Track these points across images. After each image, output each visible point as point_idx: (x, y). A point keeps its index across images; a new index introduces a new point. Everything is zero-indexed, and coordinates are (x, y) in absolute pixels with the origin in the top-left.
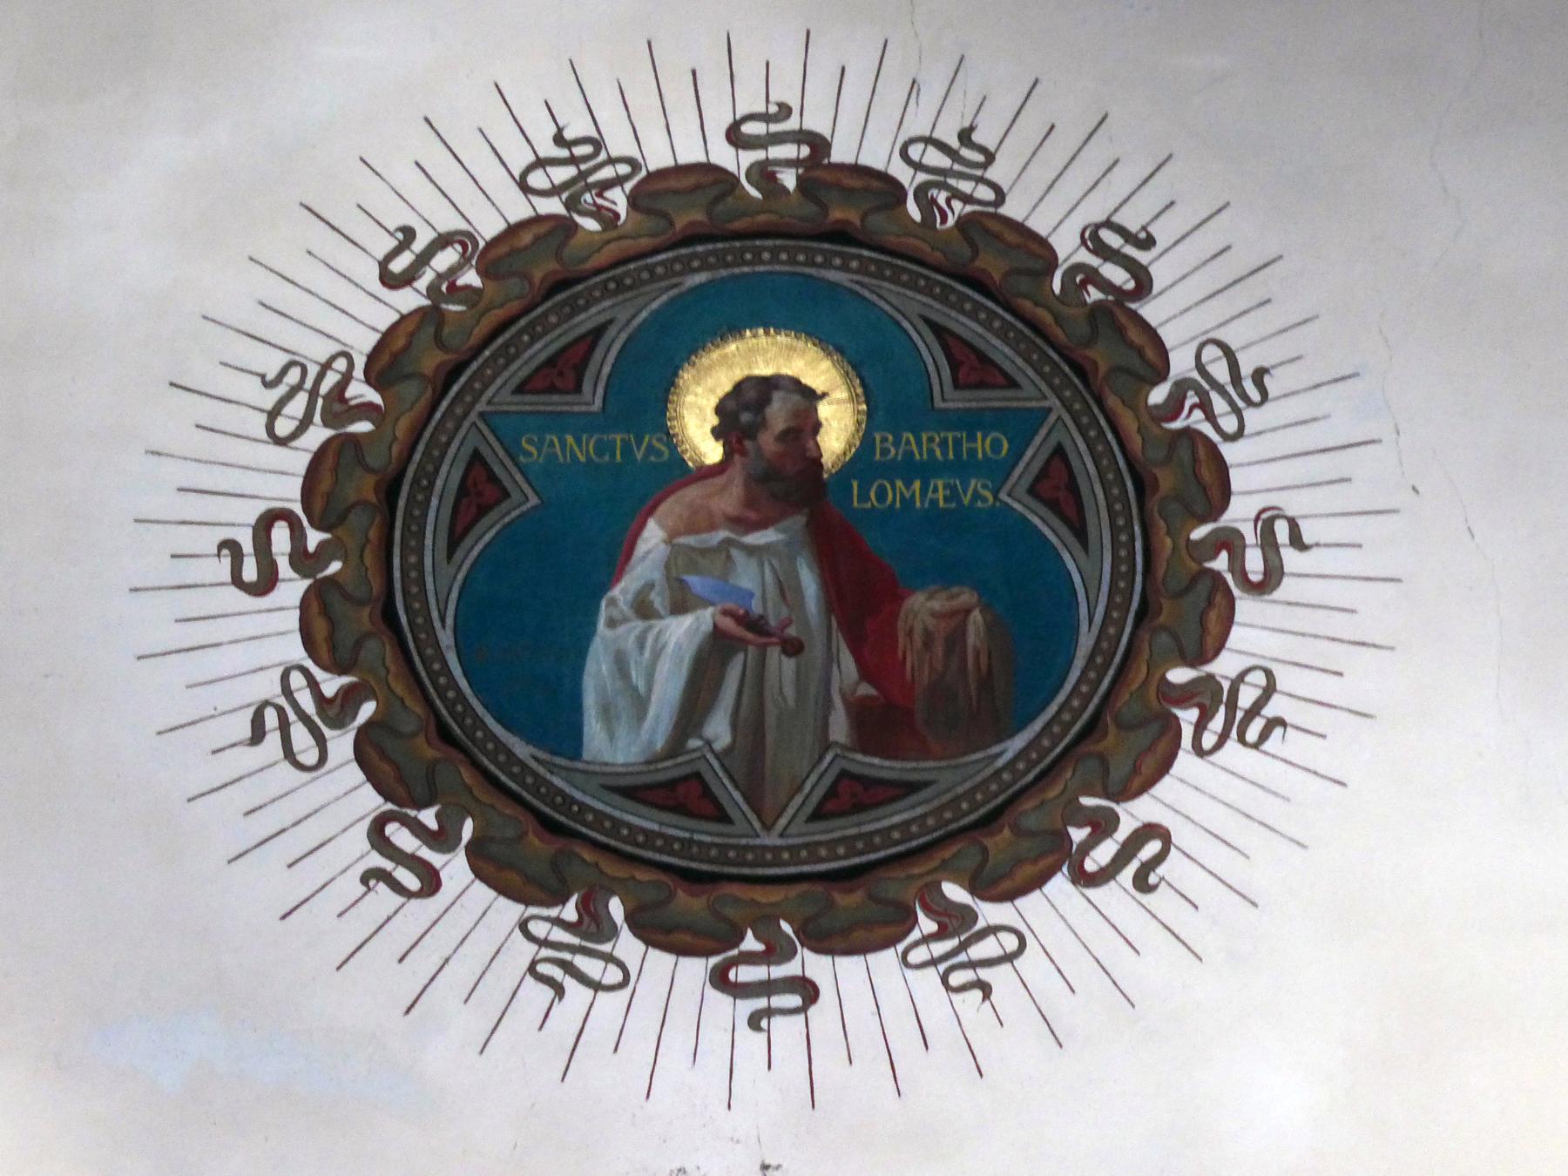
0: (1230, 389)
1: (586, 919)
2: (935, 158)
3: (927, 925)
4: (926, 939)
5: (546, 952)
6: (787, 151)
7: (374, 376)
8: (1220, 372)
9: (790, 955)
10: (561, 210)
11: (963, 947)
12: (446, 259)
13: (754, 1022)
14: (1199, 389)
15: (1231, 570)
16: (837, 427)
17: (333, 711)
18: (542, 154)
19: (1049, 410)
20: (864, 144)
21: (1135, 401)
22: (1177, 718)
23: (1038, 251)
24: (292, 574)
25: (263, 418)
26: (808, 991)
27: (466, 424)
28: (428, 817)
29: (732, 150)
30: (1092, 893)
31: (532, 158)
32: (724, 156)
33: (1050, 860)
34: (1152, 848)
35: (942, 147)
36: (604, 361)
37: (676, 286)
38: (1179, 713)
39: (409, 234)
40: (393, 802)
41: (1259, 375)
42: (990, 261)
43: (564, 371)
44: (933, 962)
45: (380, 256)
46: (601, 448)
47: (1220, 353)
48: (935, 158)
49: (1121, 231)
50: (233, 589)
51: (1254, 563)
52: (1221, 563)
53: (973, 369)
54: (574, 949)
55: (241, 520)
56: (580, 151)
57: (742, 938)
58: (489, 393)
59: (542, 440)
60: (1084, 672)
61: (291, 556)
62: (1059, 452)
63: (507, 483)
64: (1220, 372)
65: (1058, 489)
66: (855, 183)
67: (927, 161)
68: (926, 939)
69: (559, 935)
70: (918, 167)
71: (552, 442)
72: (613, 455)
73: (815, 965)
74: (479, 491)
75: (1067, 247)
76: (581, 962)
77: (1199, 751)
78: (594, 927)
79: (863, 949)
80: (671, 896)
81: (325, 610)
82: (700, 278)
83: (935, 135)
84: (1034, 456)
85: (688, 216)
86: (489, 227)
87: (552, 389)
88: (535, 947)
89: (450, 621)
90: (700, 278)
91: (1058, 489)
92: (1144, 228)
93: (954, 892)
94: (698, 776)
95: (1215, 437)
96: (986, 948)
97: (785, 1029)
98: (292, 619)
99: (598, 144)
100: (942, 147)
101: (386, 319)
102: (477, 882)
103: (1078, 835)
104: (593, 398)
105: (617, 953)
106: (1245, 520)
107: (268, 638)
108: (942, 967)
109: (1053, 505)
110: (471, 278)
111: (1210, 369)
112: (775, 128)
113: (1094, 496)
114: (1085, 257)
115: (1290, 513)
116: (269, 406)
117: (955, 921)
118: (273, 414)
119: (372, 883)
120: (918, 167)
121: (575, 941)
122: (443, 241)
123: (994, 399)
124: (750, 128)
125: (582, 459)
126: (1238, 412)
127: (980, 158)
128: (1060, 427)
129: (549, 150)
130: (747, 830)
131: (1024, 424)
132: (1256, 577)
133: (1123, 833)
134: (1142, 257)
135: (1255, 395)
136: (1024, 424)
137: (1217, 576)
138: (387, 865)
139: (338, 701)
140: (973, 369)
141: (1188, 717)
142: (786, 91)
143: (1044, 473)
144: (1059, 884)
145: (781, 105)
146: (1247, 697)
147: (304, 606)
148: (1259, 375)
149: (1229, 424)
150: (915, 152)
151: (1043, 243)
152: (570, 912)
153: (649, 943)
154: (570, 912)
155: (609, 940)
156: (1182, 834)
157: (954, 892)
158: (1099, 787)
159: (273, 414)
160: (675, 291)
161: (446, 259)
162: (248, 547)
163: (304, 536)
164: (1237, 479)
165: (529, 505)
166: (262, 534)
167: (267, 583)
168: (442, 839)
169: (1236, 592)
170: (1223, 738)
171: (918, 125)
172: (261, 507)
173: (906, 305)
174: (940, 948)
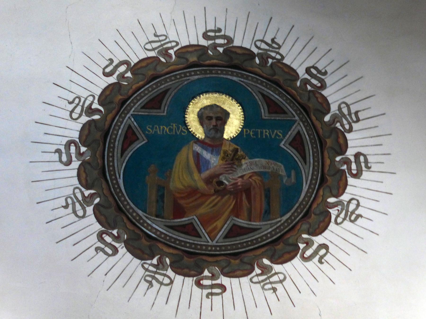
2: (264, 46)
3: (258, 271)
4: (257, 275)
6: (206, 282)
7: (100, 103)
11: (269, 278)
12: (123, 68)
15: (348, 169)
18: (280, 285)
20: (242, 40)
21: (321, 120)
22: (330, 213)
24: (76, 159)
25: (69, 113)
26: (205, 36)
28: (309, 88)
29: (223, 283)
31: (284, 283)
33: (136, 68)
35: (157, 281)
36: (167, 100)
38: (330, 210)
40: (105, 228)
41: (356, 113)
42: (280, 76)
43: (155, 102)
45: (103, 67)
46: (171, 130)
48: (264, 46)
49: (106, 253)
50: (59, 163)
53: (274, 107)
56: (161, 38)
57: (224, 51)
59: (153, 126)
60: (305, 197)
67: (262, 47)
68: (257, 275)
71: (156, 127)
73: (204, 42)
74: (130, 137)
75: (301, 72)
76: (267, 47)
77: (336, 223)
80: (183, 258)
81: (340, 145)
82: (196, 77)
84: (292, 133)
85: (193, 59)
86: (134, 60)
87: (153, 108)
90: (196, 77)
92: (97, 253)
94: (192, 223)
96: (275, 278)
97: (217, 299)
100: (157, 281)
104: (164, 112)
106: (75, 161)
107: (68, 178)
108: (262, 284)
110: (129, 74)
114: (307, 76)
116: (70, 110)
117: (265, 270)
118: (72, 112)
119: (98, 251)
122: (122, 63)
123: (279, 117)
128: (300, 127)
129: (279, 286)
130: (205, 239)
134: (100, 245)
138: (102, 246)
140: (274, 107)
142: (207, 302)
147: (79, 169)
148: (356, 113)
150: (258, 44)
151: (295, 71)
157: (266, 262)
159: (72, 112)
161: (123, 68)
166: (67, 147)
168: (306, 82)
170: (344, 219)
171: (259, 36)
174: (261, 278)
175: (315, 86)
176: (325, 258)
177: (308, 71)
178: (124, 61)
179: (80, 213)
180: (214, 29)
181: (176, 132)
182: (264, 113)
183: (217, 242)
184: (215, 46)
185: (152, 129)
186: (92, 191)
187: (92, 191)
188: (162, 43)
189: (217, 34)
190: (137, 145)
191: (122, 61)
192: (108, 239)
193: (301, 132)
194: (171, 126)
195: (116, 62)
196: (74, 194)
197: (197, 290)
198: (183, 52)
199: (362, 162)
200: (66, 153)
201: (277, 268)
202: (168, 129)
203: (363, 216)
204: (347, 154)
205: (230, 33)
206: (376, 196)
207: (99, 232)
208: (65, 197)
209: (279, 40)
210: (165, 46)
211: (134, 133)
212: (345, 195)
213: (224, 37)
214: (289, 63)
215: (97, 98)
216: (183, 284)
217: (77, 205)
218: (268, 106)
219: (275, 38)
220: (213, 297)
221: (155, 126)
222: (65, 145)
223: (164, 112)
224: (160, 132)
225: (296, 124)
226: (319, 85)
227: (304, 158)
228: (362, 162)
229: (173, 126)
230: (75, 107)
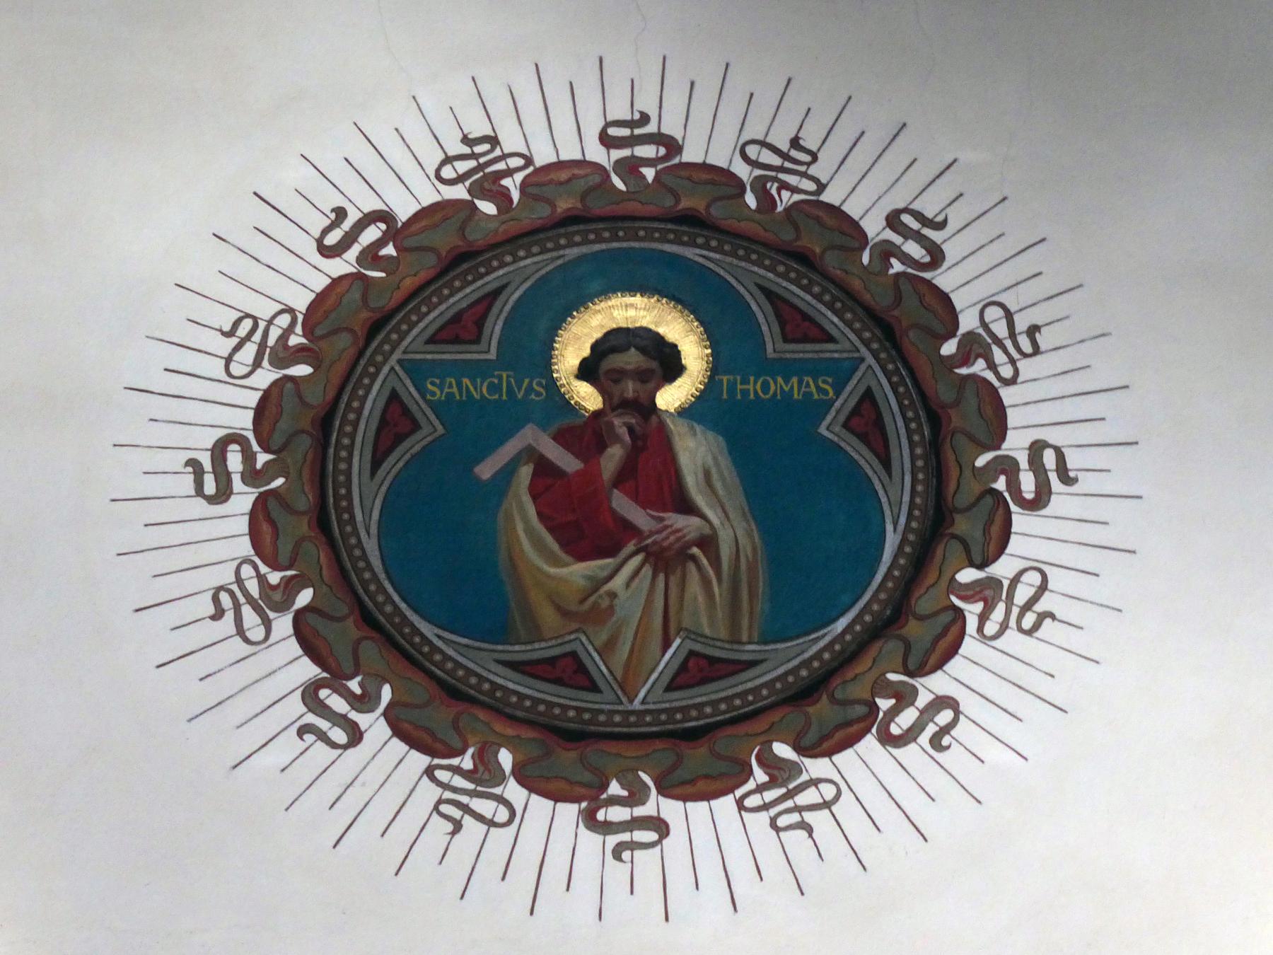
0: (242, 600)
1: (481, 769)
5: (448, 795)
6: (617, 814)
8: (1001, 329)
9: (619, 163)
10: (466, 196)
13: (645, 119)
14: (974, 347)
16: (670, 397)
17: (976, 349)
19: (862, 360)
20: (707, 145)
23: (851, 230)
27: (386, 369)
30: (379, 206)
31: (834, 808)
32: (671, 809)
34: (332, 239)
35: (480, 818)
37: (559, 258)
39: (341, 213)
42: (812, 242)
44: (765, 807)
46: (494, 388)
47: (248, 634)
51: (235, 461)
52: (262, 458)
53: (799, 326)
54: (781, 169)
55: (1062, 500)
58: (405, 343)
61: (1019, 470)
62: (868, 395)
63: (419, 416)
64: (1001, 329)
65: (867, 421)
66: (705, 176)
69: (459, 782)
70: (754, 164)
72: (501, 395)
74: (396, 422)
78: (485, 775)
79: (708, 796)
83: (769, 140)
86: (404, 210)
88: (439, 790)
89: (374, 529)
91: (867, 421)
93: (782, 750)
95: (996, 383)
98: (243, 525)
99: (494, 141)
101: (320, 283)
102: (856, 218)
103: (389, 250)
105: (506, 796)
109: (863, 438)
111: (993, 327)
112: (625, 837)
113: (896, 426)
115: (201, 500)
117: (779, 772)
120: (754, 164)
121: (471, 786)
124: (649, 836)
125: (477, 396)
126: (1013, 362)
127: (807, 158)
128: (873, 373)
131: (841, 374)
132: (1029, 496)
133: (355, 250)
135: (224, 597)
136: (841, 374)
137: (998, 494)
139: (973, 356)
140: (799, 326)
141: (972, 610)
142: (617, 872)
143: (856, 412)
144: (869, 743)
145: (642, 113)
146: (1022, 594)
148: (218, 614)
149: (1007, 372)
150: (752, 151)
151: (855, 225)
152: (467, 763)
153: (531, 790)
154: (467, 763)
155: (499, 785)
156: (968, 703)
157: (782, 750)
158: (901, 670)
160: (560, 262)
162: (207, 465)
163: (1009, 484)
164: (1013, 418)
165: (436, 435)
167: (224, 493)
169: (1013, 508)
171: (755, 130)
172: (221, 433)
173: (745, 276)
175: (335, 691)
176: (327, 222)
177: (893, 220)
178: (374, 211)
179: (257, 633)
180: (629, 118)
181: (510, 391)
182: (773, 345)
183: (643, 702)
184: (630, 168)
185: (441, 387)
186: (964, 371)
187: (964, 371)
188: (789, 804)
189: (637, 131)
190: (414, 445)
191: (370, 213)
192: (914, 249)
193: (875, 389)
194: (493, 376)
195: (353, 217)
196: (239, 581)
197: (590, 841)
198: (545, 179)
199: (1052, 470)
200: (1046, 471)
201: (816, 767)
202: (485, 384)
203: (1058, 616)
204: (252, 498)
205: (672, 127)
206: (1086, 559)
207: (941, 266)
208: (211, 592)
209: (811, 142)
210: (489, 170)
211: (406, 412)
212: (1003, 559)
213: (658, 139)
214: (415, 754)
215: (300, 318)
216: (549, 823)
217: (247, 611)
218: (782, 323)
219: (453, 833)
220: (637, 853)
221: (448, 380)
222: (213, 450)
223: (488, 351)
224: (461, 395)
225: (863, 367)
226: (323, 693)
227: (886, 463)
228: (1052, 470)
229: (500, 378)
230: (237, 348)
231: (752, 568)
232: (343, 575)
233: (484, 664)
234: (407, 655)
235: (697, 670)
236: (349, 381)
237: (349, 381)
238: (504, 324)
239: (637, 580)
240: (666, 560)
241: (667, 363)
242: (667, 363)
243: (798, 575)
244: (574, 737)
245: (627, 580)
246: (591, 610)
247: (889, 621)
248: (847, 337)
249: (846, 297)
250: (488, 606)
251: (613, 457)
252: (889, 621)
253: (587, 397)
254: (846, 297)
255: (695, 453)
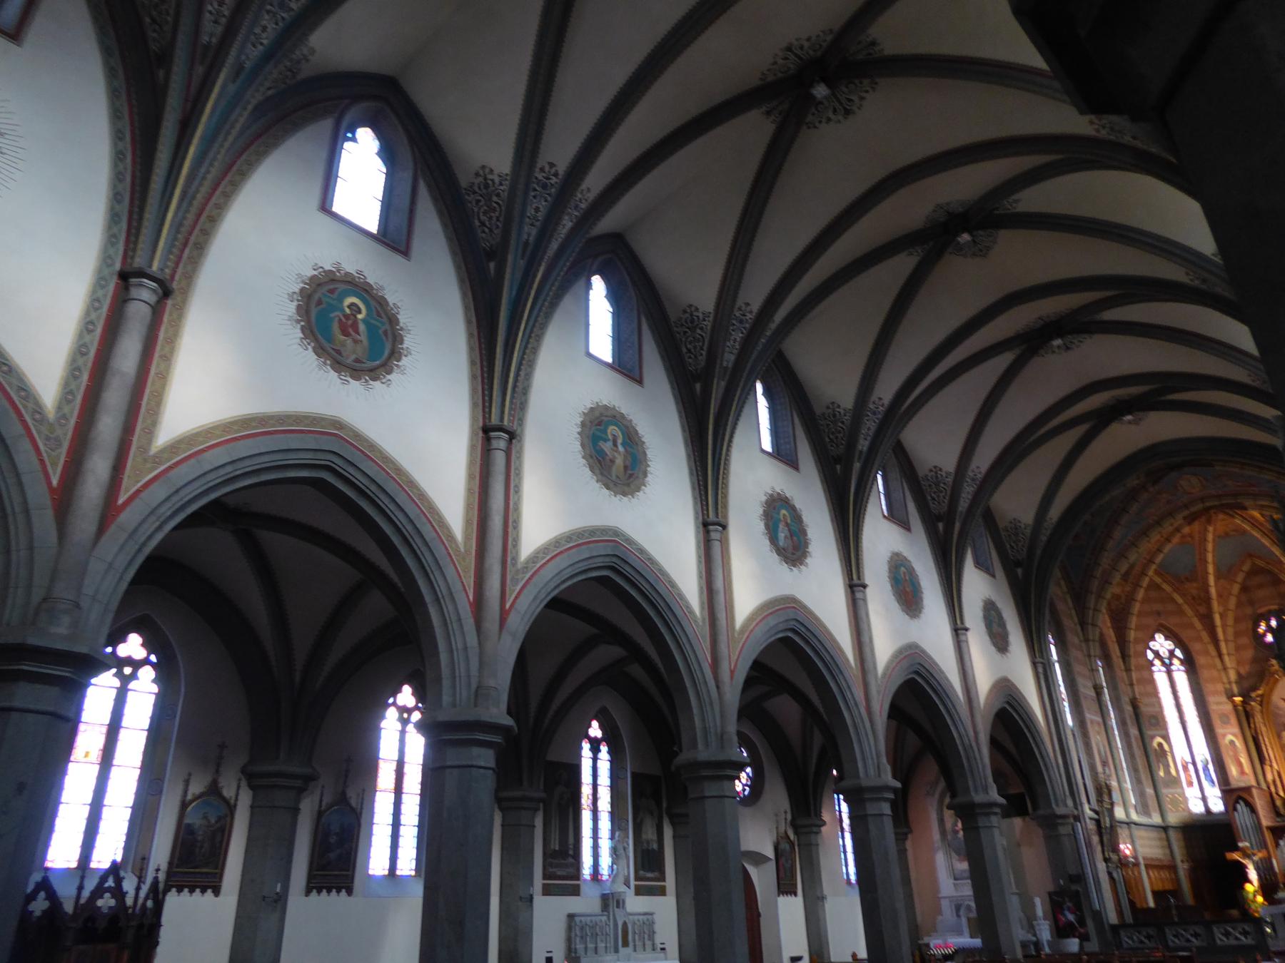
16: (360, 316)
20: (371, 280)
65: (385, 333)
74: (319, 303)
91: (385, 333)
128: (387, 327)
173: (373, 303)
198: (347, 274)
231: (1206, 769)
232: (309, 322)
233: (327, 346)
234: (316, 340)
235: (357, 361)
236: (315, 291)
237: (315, 291)
238: (503, 849)
239: (149, 533)
240: (356, 341)
241: (360, 312)
242: (360, 312)
243: (374, 352)
244: (339, 363)
245: (349, 341)
246: (343, 345)
247: (384, 365)
248: (385, 320)
249: (386, 314)
250: (330, 339)
251: (350, 322)
252: (384, 365)
253: (348, 311)
254: (386, 314)
255: (362, 327)
